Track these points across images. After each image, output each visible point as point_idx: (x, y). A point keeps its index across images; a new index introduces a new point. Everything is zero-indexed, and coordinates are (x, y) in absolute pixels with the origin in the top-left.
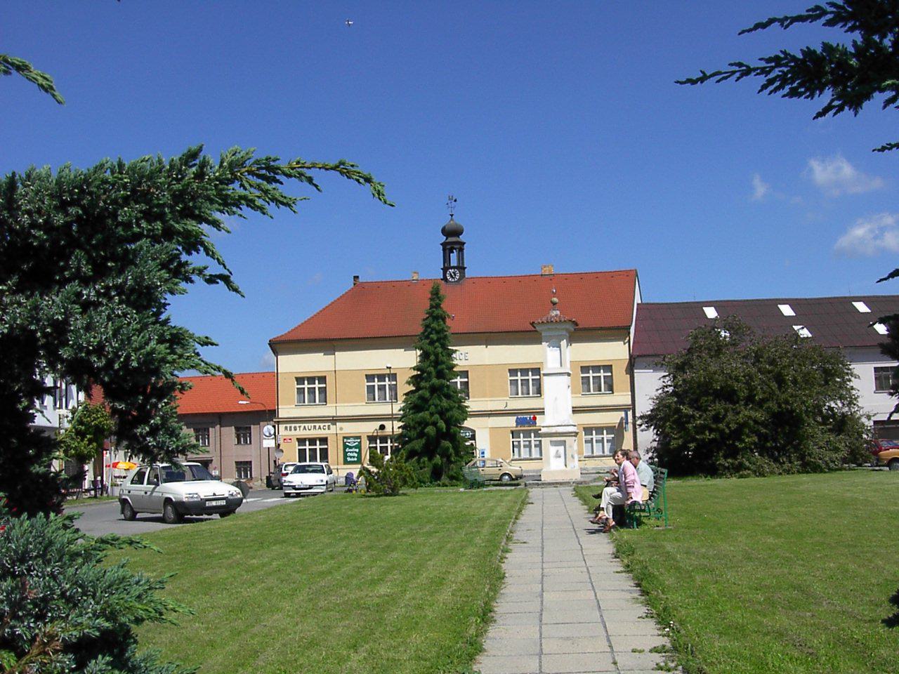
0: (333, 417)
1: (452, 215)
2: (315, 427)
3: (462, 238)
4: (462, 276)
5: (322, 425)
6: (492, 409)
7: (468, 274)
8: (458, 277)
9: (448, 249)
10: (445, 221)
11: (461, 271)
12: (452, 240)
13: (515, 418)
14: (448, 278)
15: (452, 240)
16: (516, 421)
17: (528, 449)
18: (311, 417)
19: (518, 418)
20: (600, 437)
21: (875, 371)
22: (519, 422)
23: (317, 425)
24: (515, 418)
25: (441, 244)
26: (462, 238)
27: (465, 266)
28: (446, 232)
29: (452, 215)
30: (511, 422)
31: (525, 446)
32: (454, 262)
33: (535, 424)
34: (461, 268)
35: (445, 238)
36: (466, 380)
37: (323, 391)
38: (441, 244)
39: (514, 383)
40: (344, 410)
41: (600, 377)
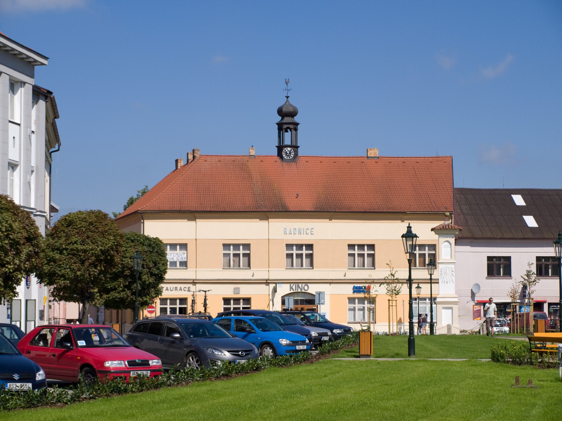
0: (267, 280)
1: (287, 97)
2: (176, 289)
3: (296, 119)
4: (296, 155)
5: (183, 286)
6: (333, 278)
7: (301, 152)
8: (292, 156)
9: (281, 128)
10: (281, 102)
11: (296, 149)
12: (287, 120)
13: (352, 286)
14: (284, 156)
15: (287, 120)
16: (353, 289)
17: (362, 312)
18: (218, 280)
19: (354, 287)
20: (361, 306)
21: (537, 261)
22: (356, 290)
23: (179, 286)
24: (352, 286)
25: (277, 124)
26: (296, 119)
27: (298, 145)
28: (280, 112)
29: (287, 97)
30: (348, 290)
31: (359, 310)
32: (287, 141)
33: (369, 292)
34: (295, 147)
35: (280, 118)
36: (311, 252)
37: (310, 256)
38: (277, 124)
39: (290, 256)
40: (201, 275)
41: (230, 254)
